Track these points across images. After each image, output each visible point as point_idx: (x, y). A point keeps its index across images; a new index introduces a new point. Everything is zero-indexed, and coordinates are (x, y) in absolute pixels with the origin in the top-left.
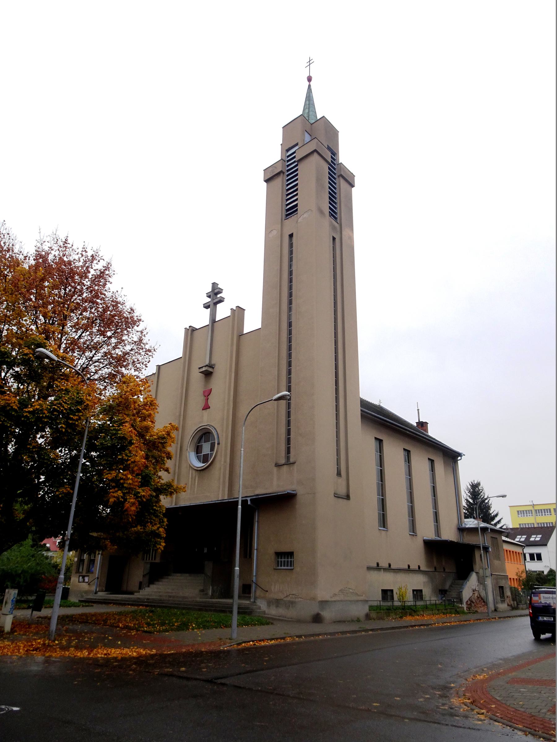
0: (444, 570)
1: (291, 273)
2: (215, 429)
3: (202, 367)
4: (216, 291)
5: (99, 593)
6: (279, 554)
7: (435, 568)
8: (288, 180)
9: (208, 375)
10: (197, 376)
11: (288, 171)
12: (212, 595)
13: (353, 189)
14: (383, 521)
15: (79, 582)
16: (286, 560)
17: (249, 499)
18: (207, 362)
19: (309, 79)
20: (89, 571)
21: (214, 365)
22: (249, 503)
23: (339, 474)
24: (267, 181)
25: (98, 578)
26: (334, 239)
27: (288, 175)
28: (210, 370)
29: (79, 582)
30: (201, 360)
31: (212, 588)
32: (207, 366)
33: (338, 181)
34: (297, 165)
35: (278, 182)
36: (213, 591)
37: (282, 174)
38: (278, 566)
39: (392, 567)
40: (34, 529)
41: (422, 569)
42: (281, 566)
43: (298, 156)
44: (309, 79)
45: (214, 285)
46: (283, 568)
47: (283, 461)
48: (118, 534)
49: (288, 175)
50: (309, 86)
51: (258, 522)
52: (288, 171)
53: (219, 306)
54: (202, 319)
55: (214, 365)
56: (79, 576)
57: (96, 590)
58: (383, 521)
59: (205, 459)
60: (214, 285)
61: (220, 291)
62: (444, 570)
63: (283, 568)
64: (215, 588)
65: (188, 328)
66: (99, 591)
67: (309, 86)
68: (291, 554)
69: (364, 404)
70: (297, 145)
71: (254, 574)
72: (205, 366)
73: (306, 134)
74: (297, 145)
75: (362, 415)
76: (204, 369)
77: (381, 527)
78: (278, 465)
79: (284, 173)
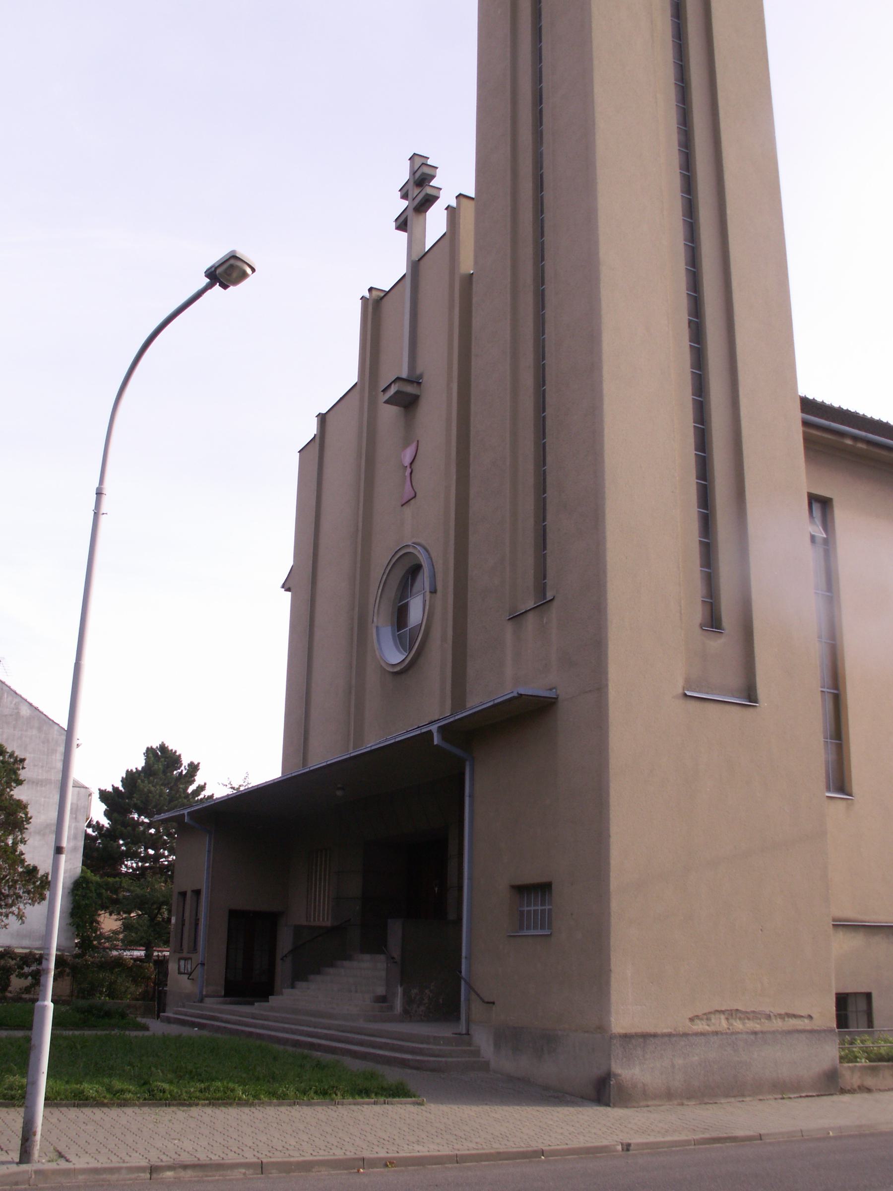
1: (538, 98)
3: (390, 385)
5: (207, 1000)
6: (522, 890)
9: (407, 402)
10: (389, 414)
12: (406, 1012)
15: (180, 973)
16: (532, 908)
17: (434, 728)
20: (195, 949)
21: (421, 376)
25: (203, 964)
28: (410, 389)
31: (405, 993)
36: (409, 1001)
38: (521, 928)
40: (152, 831)
42: (528, 928)
46: (532, 932)
48: (123, 848)
56: (180, 959)
57: (201, 992)
63: (532, 932)
64: (415, 991)
65: (367, 295)
66: (207, 996)
68: (544, 889)
69: (808, 405)
72: (394, 382)
75: (808, 441)
76: (393, 390)
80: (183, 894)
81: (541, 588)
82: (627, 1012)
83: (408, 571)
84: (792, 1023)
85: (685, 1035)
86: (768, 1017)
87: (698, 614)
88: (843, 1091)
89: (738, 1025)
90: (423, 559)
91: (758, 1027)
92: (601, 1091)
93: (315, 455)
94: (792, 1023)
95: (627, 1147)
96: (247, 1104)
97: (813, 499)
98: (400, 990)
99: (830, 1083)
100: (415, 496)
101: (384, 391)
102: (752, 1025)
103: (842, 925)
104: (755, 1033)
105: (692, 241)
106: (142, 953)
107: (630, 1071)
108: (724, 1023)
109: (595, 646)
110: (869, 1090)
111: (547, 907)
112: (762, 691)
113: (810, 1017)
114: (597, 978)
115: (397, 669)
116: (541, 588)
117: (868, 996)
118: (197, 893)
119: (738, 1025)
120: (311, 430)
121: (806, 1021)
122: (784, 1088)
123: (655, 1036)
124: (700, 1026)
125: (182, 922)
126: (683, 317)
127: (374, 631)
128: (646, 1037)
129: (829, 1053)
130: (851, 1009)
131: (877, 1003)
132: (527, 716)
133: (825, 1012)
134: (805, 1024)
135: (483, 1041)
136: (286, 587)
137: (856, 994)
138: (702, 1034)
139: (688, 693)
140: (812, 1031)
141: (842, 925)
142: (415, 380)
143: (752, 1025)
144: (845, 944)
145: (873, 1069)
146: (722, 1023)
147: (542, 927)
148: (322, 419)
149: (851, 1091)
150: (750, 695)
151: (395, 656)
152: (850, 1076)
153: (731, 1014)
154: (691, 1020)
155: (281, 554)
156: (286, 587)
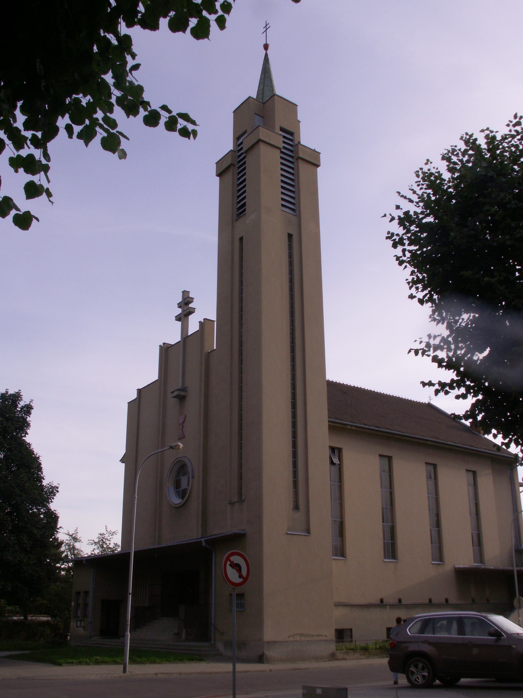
0: (488, 600)
2: (190, 460)
4: (186, 301)
7: (473, 600)
8: (239, 173)
9: (181, 398)
10: (172, 402)
11: (239, 162)
13: (318, 169)
14: (391, 550)
15: (77, 627)
18: (180, 386)
19: (266, 47)
20: (85, 616)
21: (187, 388)
22: (204, 544)
23: (296, 507)
24: (220, 175)
25: (91, 623)
26: (290, 236)
27: (239, 168)
28: (183, 393)
29: (77, 627)
30: (175, 384)
32: (178, 390)
33: (298, 163)
34: (245, 157)
35: (229, 176)
37: (232, 167)
39: (403, 602)
41: (450, 602)
43: (245, 147)
44: (266, 47)
45: (185, 294)
47: (236, 499)
49: (239, 168)
50: (266, 55)
51: (215, 563)
52: (239, 162)
53: (191, 317)
54: (174, 337)
55: (187, 388)
56: (77, 621)
58: (391, 550)
59: (182, 494)
60: (185, 294)
61: (191, 300)
62: (488, 600)
65: (202, 321)
67: (266, 55)
70: (245, 132)
71: (213, 617)
73: (257, 117)
74: (245, 132)
76: (176, 393)
77: (388, 558)
78: (232, 504)
79: (234, 165)
80: (78, 593)
81: (240, 494)
82: (269, 635)
83: (181, 468)
84: (321, 638)
85: (287, 641)
86: (313, 636)
87: (291, 506)
88: (336, 659)
89: (303, 638)
90: (186, 460)
91: (309, 639)
92: (261, 659)
93: (136, 408)
94: (321, 638)
95: (271, 671)
96: (160, 663)
97: (333, 449)
98: (184, 630)
99: (333, 657)
100: (184, 437)
101: (172, 392)
102: (307, 638)
103: (338, 605)
104: (308, 641)
105: (292, 317)
106: (23, 618)
107: (269, 653)
108: (299, 638)
109: (259, 517)
110: (345, 659)
111: (242, 602)
112: (312, 531)
113: (326, 636)
114: (259, 624)
115: (177, 506)
116: (240, 494)
117: (351, 630)
118: (86, 593)
119: (303, 638)
120: (134, 396)
121: (325, 637)
122: (317, 659)
123: (277, 642)
124: (291, 639)
125: (78, 605)
126: (290, 401)
127: (167, 489)
128: (275, 642)
129: (332, 647)
130: (342, 635)
131: (354, 632)
132: (235, 540)
133: (331, 635)
134: (325, 638)
135: (220, 646)
136: (122, 461)
137: (347, 629)
138: (292, 641)
139: (288, 532)
140: (327, 641)
141: (338, 605)
142: (184, 389)
143: (307, 638)
144: (339, 612)
145: (347, 653)
146: (298, 638)
147: (241, 608)
148: (139, 391)
149: (339, 660)
150: (308, 531)
151: (177, 501)
152: (339, 655)
153: (301, 635)
154: (288, 637)
155: (122, 451)
156: (122, 461)
